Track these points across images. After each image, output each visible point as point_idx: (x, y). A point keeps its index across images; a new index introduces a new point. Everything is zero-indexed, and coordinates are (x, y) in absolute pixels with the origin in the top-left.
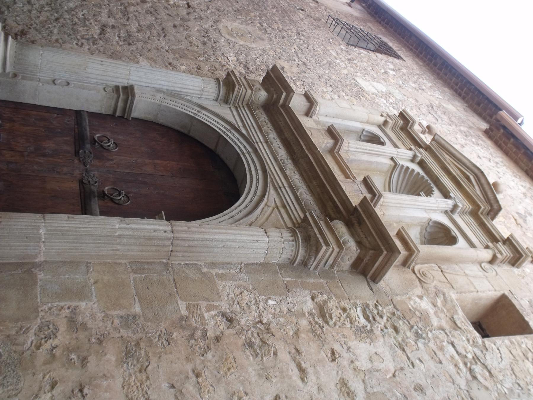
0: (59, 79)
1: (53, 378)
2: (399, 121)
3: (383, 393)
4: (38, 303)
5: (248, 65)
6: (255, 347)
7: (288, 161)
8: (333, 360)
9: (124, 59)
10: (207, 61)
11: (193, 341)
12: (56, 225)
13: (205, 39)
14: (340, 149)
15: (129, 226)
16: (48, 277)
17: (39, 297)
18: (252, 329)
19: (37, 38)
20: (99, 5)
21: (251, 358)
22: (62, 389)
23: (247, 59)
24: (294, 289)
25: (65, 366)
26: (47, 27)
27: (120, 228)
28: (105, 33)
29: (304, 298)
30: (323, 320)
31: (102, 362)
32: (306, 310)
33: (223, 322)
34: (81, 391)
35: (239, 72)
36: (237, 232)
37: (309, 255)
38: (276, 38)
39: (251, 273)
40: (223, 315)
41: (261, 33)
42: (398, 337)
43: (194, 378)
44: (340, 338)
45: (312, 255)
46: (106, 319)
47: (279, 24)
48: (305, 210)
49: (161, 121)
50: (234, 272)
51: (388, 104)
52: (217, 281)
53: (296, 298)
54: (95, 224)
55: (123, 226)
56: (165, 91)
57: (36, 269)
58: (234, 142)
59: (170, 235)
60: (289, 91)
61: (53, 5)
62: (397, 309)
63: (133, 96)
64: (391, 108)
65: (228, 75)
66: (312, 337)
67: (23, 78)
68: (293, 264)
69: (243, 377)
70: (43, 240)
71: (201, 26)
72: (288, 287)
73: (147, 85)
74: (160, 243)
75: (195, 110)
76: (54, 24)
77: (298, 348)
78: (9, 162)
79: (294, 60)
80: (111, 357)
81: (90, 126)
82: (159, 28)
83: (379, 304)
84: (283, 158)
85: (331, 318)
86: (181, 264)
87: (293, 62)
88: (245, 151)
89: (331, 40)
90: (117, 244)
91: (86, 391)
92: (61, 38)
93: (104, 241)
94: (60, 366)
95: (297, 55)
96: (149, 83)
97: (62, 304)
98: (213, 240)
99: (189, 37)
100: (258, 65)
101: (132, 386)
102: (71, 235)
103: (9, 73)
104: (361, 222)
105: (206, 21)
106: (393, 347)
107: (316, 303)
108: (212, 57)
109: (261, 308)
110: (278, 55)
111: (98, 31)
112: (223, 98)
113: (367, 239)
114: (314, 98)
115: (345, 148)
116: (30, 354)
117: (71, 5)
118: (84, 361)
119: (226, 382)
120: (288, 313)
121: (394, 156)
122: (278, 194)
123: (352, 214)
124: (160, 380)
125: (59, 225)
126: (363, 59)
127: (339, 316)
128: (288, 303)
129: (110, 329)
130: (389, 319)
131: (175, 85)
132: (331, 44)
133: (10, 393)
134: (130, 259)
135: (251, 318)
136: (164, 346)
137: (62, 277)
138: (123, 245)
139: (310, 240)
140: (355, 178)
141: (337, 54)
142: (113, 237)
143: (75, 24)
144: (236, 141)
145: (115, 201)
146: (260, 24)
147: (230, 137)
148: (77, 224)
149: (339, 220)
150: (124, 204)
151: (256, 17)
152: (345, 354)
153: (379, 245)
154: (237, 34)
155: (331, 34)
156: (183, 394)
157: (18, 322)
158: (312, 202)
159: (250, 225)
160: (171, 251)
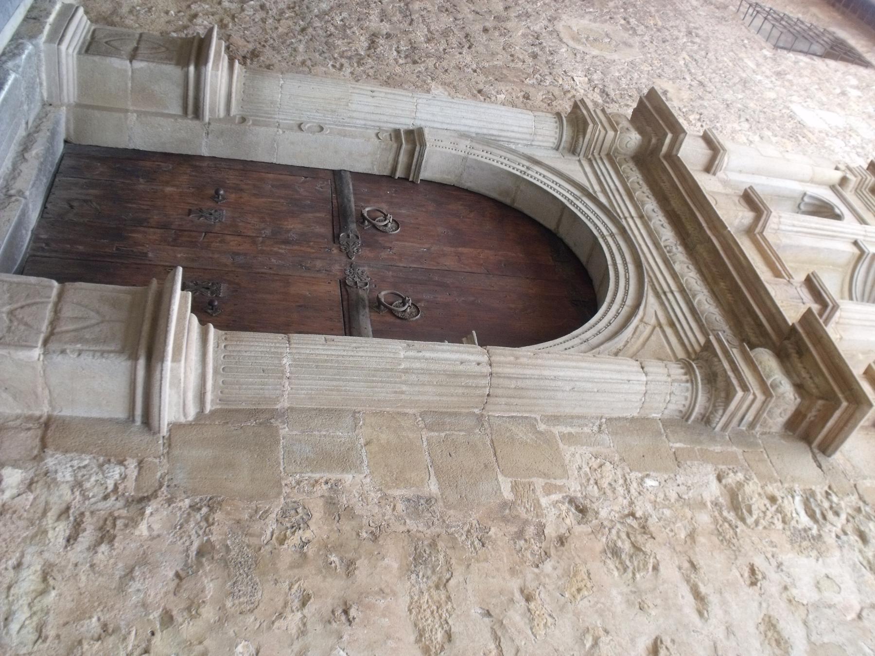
0: (308, 123)
1: (304, 591)
2: (869, 178)
3: (840, 647)
4: (281, 473)
5: (606, 89)
6: (623, 556)
7: (677, 249)
8: (753, 584)
9: (406, 87)
10: (539, 84)
11: (522, 542)
12: (308, 352)
13: (536, 49)
14: (764, 227)
15: (420, 354)
16: (295, 433)
17: (282, 463)
18: (618, 526)
19: (274, 61)
20: (365, 3)
21: (616, 573)
22: (317, 607)
23: (606, 80)
24: (689, 463)
25: (321, 572)
26: (288, 42)
27: (406, 358)
28: (375, 46)
29: (704, 478)
30: (737, 515)
31: (378, 569)
32: (708, 498)
33: (571, 514)
34: (346, 612)
35: (593, 101)
36: (595, 366)
37: (714, 406)
38: (652, 42)
39: (617, 434)
40: (572, 501)
41: (626, 35)
42: (865, 549)
43: (523, 603)
44: (765, 547)
45: (719, 406)
46: (383, 502)
47: (657, 18)
48: (706, 330)
49: (468, 184)
50: (589, 431)
51: (848, 149)
52: (561, 445)
53: (692, 476)
54: (366, 351)
55: (411, 353)
56: (474, 135)
57: (277, 420)
58: (587, 218)
59: (487, 369)
60: (678, 131)
61: (297, 8)
62: (864, 502)
63: (423, 144)
64: (854, 155)
65: (576, 106)
66: (717, 542)
67: (256, 123)
68: (687, 420)
69: (603, 604)
70: (288, 375)
71: (529, 28)
72: (677, 458)
73: (445, 126)
74: (470, 382)
75: (523, 166)
76: (299, 37)
77: (694, 560)
78: (235, 254)
79: (684, 79)
80: (392, 562)
81: (355, 194)
82: (461, 35)
83: (833, 492)
84: (668, 244)
85: (750, 512)
86: (503, 417)
87: (682, 81)
88: (605, 232)
89: (746, 41)
90: (401, 383)
91: (353, 612)
92: (310, 59)
93: (382, 377)
94: (313, 572)
95: (689, 70)
96: (448, 124)
97: (317, 476)
98: (555, 378)
99: (510, 46)
100: (624, 89)
101: (425, 610)
102: (331, 368)
103: (235, 116)
104: (802, 351)
105: (535, 20)
106: (858, 567)
107: (725, 486)
108: (546, 77)
109: (633, 491)
110: (657, 71)
111: (366, 44)
112: (567, 145)
113: (813, 380)
114: (719, 143)
115: (773, 226)
116: (269, 550)
117: (324, 6)
118: (350, 566)
119: (574, 611)
120: (678, 501)
121: (860, 239)
122: (662, 304)
123: (788, 338)
124: (468, 602)
125: (312, 352)
126: (802, 71)
127: (764, 509)
128: (679, 485)
129: (390, 519)
130: (851, 519)
131: (490, 126)
132: (746, 47)
133: (243, 606)
134: (422, 407)
135: (617, 508)
136: (475, 548)
137: (316, 433)
138: (411, 384)
139: (715, 381)
140: (790, 276)
141: (758, 65)
142: (396, 372)
143: (331, 35)
144: (591, 215)
145: (396, 314)
146: (625, 19)
147: (580, 209)
148: (340, 350)
149: (765, 348)
150: (412, 319)
151: (618, 8)
152: (773, 575)
153: (834, 391)
154: (587, 39)
155: (746, 31)
156: (505, 627)
157: (251, 501)
158: (719, 318)
159: (616, 354)
160: (488, 395)
